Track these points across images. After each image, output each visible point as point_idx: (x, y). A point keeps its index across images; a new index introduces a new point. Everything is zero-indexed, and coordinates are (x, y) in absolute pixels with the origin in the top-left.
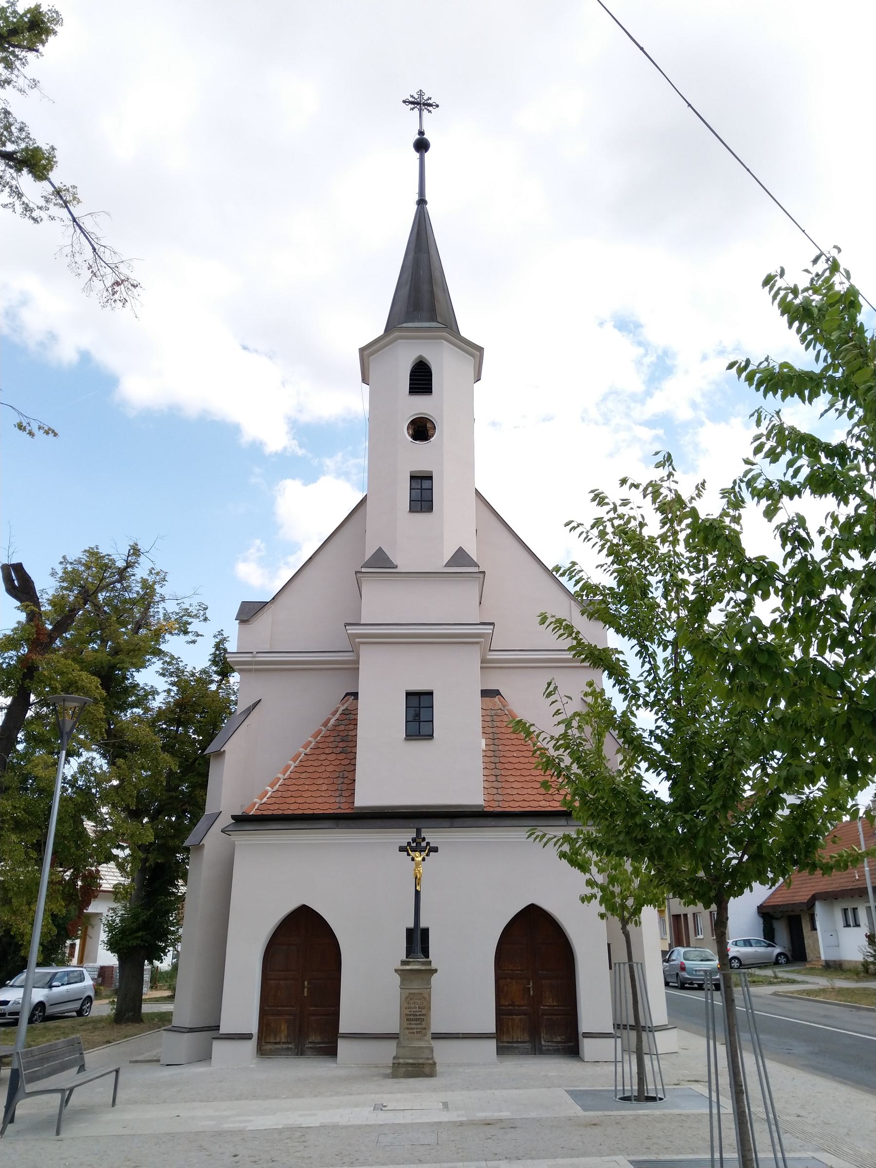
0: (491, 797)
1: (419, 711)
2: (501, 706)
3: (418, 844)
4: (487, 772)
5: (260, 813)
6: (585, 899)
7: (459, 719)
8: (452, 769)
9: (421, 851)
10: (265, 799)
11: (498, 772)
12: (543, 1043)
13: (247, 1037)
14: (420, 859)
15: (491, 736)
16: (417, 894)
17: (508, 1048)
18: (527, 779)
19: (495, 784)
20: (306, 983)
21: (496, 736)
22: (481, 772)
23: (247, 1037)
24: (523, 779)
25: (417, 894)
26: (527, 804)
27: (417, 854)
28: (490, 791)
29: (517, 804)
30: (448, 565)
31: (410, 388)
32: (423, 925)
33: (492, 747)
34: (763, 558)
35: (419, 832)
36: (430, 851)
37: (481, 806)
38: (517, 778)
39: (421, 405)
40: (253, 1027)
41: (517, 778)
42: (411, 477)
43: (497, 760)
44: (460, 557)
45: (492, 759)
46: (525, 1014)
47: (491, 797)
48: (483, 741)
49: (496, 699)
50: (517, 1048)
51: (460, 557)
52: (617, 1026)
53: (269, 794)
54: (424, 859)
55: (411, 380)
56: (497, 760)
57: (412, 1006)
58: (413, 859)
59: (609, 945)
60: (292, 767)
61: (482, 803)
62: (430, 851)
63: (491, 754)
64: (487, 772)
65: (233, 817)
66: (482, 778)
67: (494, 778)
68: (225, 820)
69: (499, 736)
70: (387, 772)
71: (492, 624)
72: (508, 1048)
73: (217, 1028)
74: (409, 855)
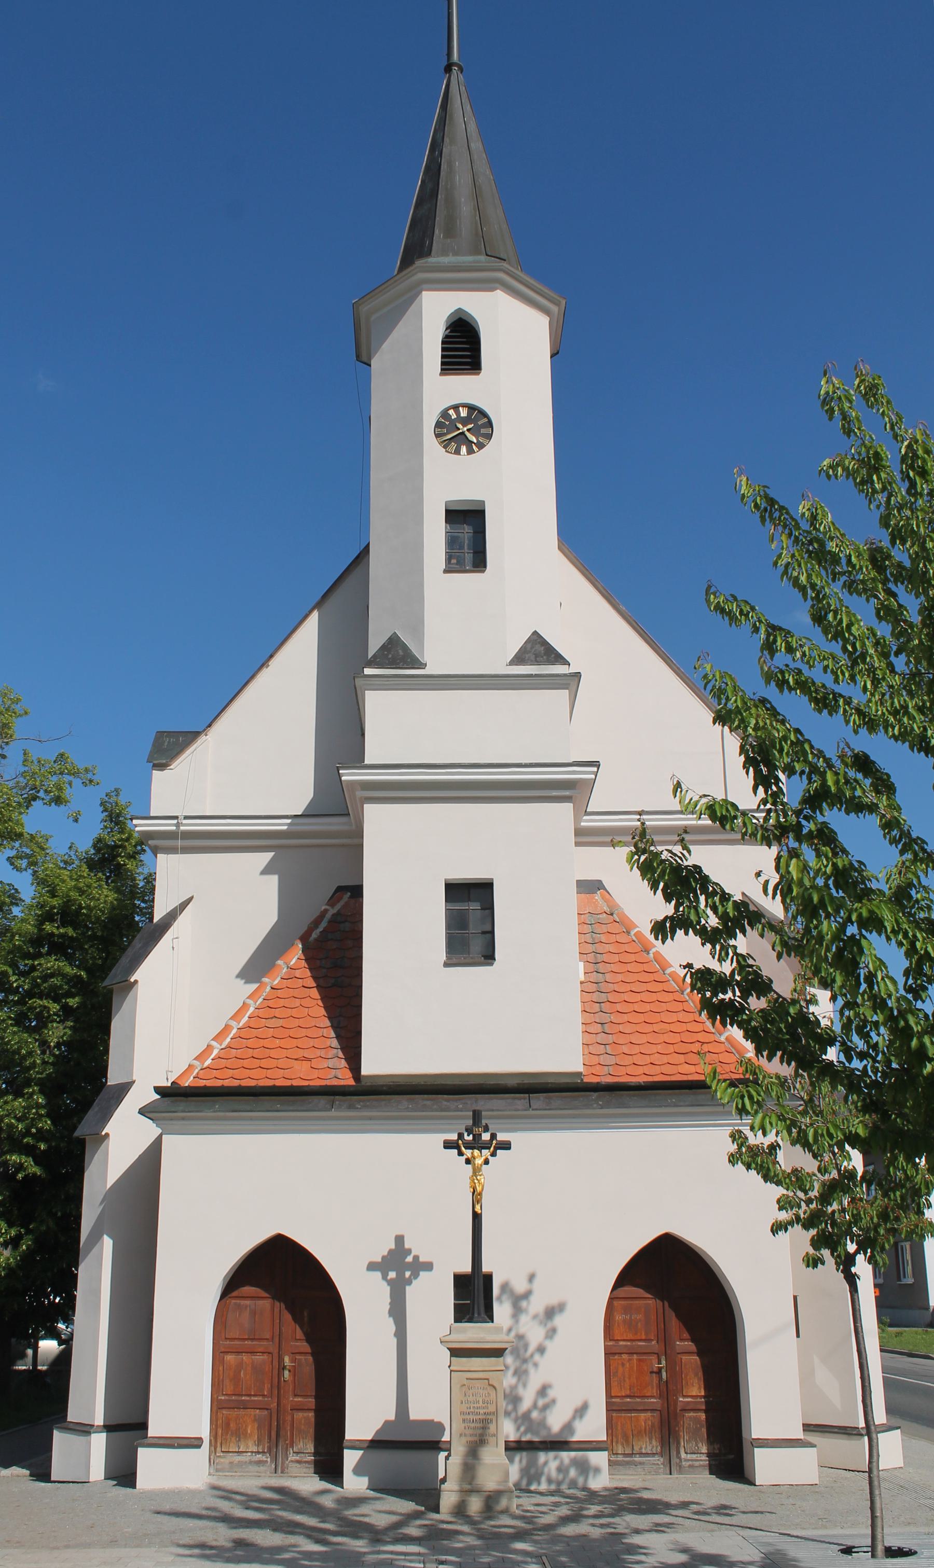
0: (595, 1060)
1: (470, 911)
2: (606, 909)
3: (477, 1137)
4: (590, 1018)
5: (202, 1083)
6: (778, 1227)
7: (537, 929)
8: (527, 1013)
9: (481, 1148)
10: (208, 1062)
11: (605, 1018)
12: (683, 1455)
13: (194, 1443)
14: (479, 1161)
15: (591, 957)
16: (477, 1218)
17: (628, 1463)
18: (656, 1028)
19: (601, 1038)
20: (287, 1359)
21: (600, 958)
22: (578, 1018)
23: (194, 1443)
24: (649, 1028)
25: (477, 1218)
26: (657, 1070)
27: (476, 1152)
28: (593, 1049)
29: (640, 1070)
30: (519, 659)
31: (443, 364)
32: (485, 1269)
33: (594, 977)
34: (836, 833)
35: (477, 1117)
36: (496, 1148)
37: (579, 1074)
38: (638, 1028)
39: (463, 389)
40: (204, 1430)
41: (638, 1028)
42: (448, 512)
43: (603, 997)
44: (538, 650)
45: (595, 997)
46: (652, 1410)
47: (595, 1060)
48: (581, 964)
49: (597, 896)
50: (641, 1463)
51: (538, 650)
52: (807, 1427)
53: (215, 1052)
54: (486, 1162)
55: (443, 349)
56: (603, 997)
57: (471, 1398)
58: (468, 1161)
59: (795, 1298)
60: (252, 1009)
61: (580, 1068)
62: (496, 1148)
63: (593, 987)
64: (590, 1018)
65: (157, 1090)
66: (580, 1028)
67: (599, 1028)
68: (142, 1094)
69: (605, 957)
70: (417, 1014)
71: (596, 764)
72: (628, 1463)
73: (143, 1426)
74: (461, 1154)
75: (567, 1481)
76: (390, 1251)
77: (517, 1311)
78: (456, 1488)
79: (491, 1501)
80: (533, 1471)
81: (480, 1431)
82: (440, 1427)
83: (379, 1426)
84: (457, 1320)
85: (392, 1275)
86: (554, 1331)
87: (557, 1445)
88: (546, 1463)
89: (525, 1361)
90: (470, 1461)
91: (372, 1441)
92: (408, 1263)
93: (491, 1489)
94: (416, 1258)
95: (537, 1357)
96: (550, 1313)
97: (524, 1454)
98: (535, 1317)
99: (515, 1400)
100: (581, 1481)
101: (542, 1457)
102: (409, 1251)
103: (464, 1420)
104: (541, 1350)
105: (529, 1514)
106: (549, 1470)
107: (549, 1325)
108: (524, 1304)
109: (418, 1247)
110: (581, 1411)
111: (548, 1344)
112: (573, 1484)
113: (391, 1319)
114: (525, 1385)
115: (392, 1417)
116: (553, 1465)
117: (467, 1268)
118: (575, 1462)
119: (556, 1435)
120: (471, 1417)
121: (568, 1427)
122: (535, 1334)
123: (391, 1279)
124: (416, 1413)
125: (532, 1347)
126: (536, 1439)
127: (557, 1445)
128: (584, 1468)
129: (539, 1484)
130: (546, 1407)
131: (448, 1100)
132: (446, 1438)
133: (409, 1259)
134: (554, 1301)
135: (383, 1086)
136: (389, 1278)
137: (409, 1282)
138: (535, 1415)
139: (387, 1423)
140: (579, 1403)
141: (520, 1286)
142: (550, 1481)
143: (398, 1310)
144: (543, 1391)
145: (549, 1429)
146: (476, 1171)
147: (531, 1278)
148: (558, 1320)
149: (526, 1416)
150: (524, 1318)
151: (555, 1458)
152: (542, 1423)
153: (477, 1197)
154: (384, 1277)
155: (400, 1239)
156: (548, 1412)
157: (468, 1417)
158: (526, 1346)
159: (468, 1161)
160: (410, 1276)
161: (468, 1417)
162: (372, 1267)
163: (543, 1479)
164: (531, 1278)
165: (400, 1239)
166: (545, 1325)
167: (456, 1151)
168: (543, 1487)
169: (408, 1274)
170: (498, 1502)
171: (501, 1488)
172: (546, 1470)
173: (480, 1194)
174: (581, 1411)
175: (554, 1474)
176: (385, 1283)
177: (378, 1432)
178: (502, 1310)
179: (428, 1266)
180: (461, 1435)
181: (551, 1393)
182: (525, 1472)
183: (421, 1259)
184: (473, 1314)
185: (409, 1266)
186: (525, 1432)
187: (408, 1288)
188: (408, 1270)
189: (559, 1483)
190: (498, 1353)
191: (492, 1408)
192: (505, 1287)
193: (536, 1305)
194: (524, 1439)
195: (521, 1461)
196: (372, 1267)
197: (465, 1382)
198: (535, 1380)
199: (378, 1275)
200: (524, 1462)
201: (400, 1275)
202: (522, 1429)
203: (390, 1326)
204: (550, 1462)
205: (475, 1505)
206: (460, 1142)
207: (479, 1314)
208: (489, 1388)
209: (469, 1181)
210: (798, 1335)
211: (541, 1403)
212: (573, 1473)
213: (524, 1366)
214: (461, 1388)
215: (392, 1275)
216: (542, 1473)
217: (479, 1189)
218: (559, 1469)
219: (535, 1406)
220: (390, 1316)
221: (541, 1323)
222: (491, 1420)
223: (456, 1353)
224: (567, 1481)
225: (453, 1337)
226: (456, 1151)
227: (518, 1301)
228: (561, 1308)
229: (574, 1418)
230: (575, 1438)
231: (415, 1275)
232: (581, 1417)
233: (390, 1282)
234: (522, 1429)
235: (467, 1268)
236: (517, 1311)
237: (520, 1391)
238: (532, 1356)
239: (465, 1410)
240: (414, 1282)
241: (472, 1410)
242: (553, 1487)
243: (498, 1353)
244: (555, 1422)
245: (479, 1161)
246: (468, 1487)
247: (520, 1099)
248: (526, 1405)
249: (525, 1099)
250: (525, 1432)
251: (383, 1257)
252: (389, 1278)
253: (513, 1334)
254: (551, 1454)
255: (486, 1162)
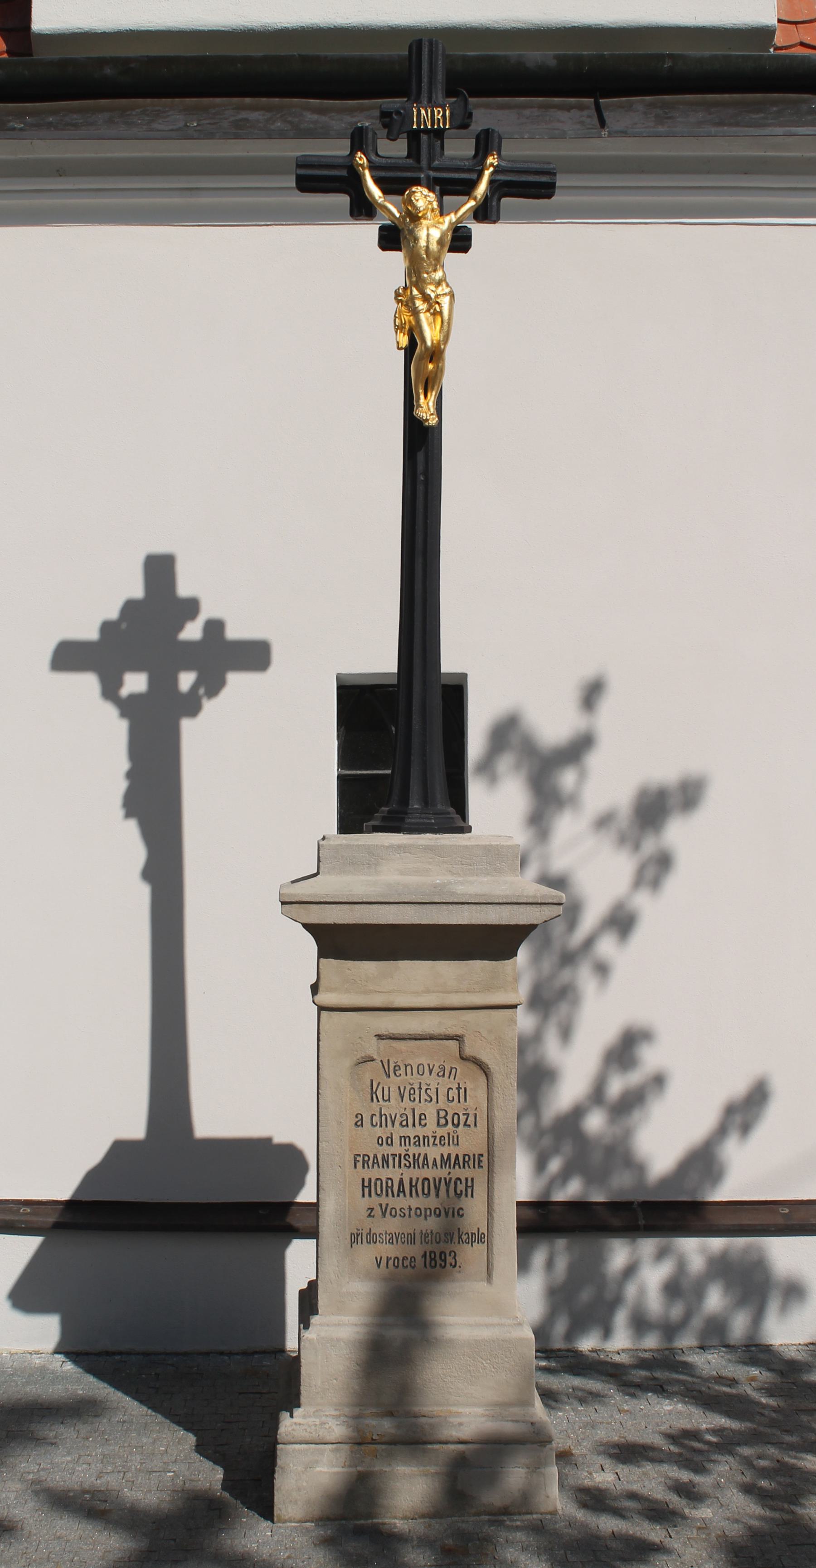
16: (421, 446)
25: (421, 446)
32: (450, 662)
37: (763, 34)
57: (394, 1107)
62: (499, 188)
75: (697, 1323)
76: (130, 607)
77: (546, 802)
78: (337, 1429)
79: (470, 1470)
80: (586, 1295)
81: (432, 1224)
82: (287, 1160)
83: (94, 1156)
84: (349, 822)
85: (135, 683)
86: (663, 862)
87: (672, 1212)
88: (630, 1271)
89: (569, 959)
90: (397, 1334)
91: (70, 1205)
92: (190, 645)
93: (466, 1433)
94: (215, 627)
95: (607, 946)
96: (654, 809)
97: (561, 1243)
98: (603, 822)
99: (536, 1079)
100: (739, 1326)
101: (618, 1254)
102: (191, 607)
103: (366, 1187)
104: (622, 922)
105: (607, 1524)
106: (642, 1291)
107: (649, 846)
108: (568, 779)
109: (221, 593)
110: (745, 1110)
111: (643, 902)
112: (714, 1333)
113: (132, 828)
114: (566, 1033)
115: (136, 1128)
116: (653, 1277)
117: (380, 658)
118: (721, 1268)
119: (666, 1182)
120: (393, 1173)
121: (703, 1161)
122: (602, 875)
123: (133, 697)
124: (218, 1113)
125: (589, 920)
126: (598, 1197)
127: (672, 1212)
128: (753, 1285)
129: (607, 1333)
130: (631, 1103)
131: (321, 111)
132: (307, 1195)
133: (192, 631)
134: (666, 772)
135: (102, 62)
136: (125, 692)
137: (191, 706)
138: (595, 1122)
139: (120, 1150)
140: (737, 1086)
141: (553, 725)
142: (640, 1323)
143: (154, 796)
144: (625, 1049)
145: (640, 1169)
146: (416, 272)
147: (592, 694)
148: (677, 833)
149: (570, 1124)
150: (567, 827)
151: (661, 1255)
152: (619, 1154)
153: (422, 364)
154: (110, 691)
155: (160, 569)
156: (636, 1115)
157: (384, 1173)
158: (572, 912)
159: (391, 239)
160: (195, 687)
161: (384, 1173)
162: (68, 657)
163: (621, 1319)
164: (592, 694)
165: (160, 569)
166: (637, 847)
167: (343, 200)
168: (620, 1343)
169: (186, 680)
170: (492, 1477)
171: (508, 1428)
172: (631, 1291)
173: (436, 354)
174: (745, 1110)
175: (655, 1303)
176: (110, 711)
177: (92, 1177)
178: (496, 805)
179: (255, 656)
180: (355, 1238)
181: (651, 1058)
182: (559, 1297)
183: (232, 633)
184: (404, 800)
185: (190, 655)
186: (564, 1176)
187: (187, 725)
188: (188, 668)
189: (670, 1330)
190: (494, 942)
191: (471, 1141)
192: (506, 732)
193: (607, 783)
194: (560, 1196)
195: (550, 1264)
196: (68, 657)
197: (372, 1048)
198: (598, 1018)
199: (88, 683)
200: (562, 1264)
201: (164, 682)
202: (555, 1165)
203: (130, 845)
204: (645, 1269)
205: (409, 1492)
206: (361, 159)
207: (426, 801)
208: (460, 1066)
209: (393, 306)
210: (293, 882)
211: (616, 1086)
212: (715, 1300)
213: (565, 975)
214: (365, 1067)
215: (135, 683)
216: (617, 1301)
217: (431, 334)
218: (672, 1289)
219: (597, 1095)
220: (128, 815)
221: (622, 840)
222: (470, 1185)
223: (338, 941)
224: (697, 1323)
225: (329, 885)
226: (343, 200)
227: (549, 771)
228: (689, 794)
229: (721, 1131)
230: (726, 1191)
231: (212, 684)
232: (746, 1129)
233: (128, 707)
234: (555, 1165)
235: (380, 658)
236: (546, 802)
237: (551, 1049)
238: (589, 943)
239: (372, 1149)
240: (209, 706)
241: (397, 1149)
242: (651, 1342)
243: (494, 942)
244: (661, 1144)
245: (431, 232)
246: (386, 1426)
247: (568, 108)
248: (569, 1091)
249: (581, 108)
250: (564, 1176)
251: (107, 627)
252: (125, 692)
253: (532, 871)
254: (648, 1245)
255: (460, 241)
